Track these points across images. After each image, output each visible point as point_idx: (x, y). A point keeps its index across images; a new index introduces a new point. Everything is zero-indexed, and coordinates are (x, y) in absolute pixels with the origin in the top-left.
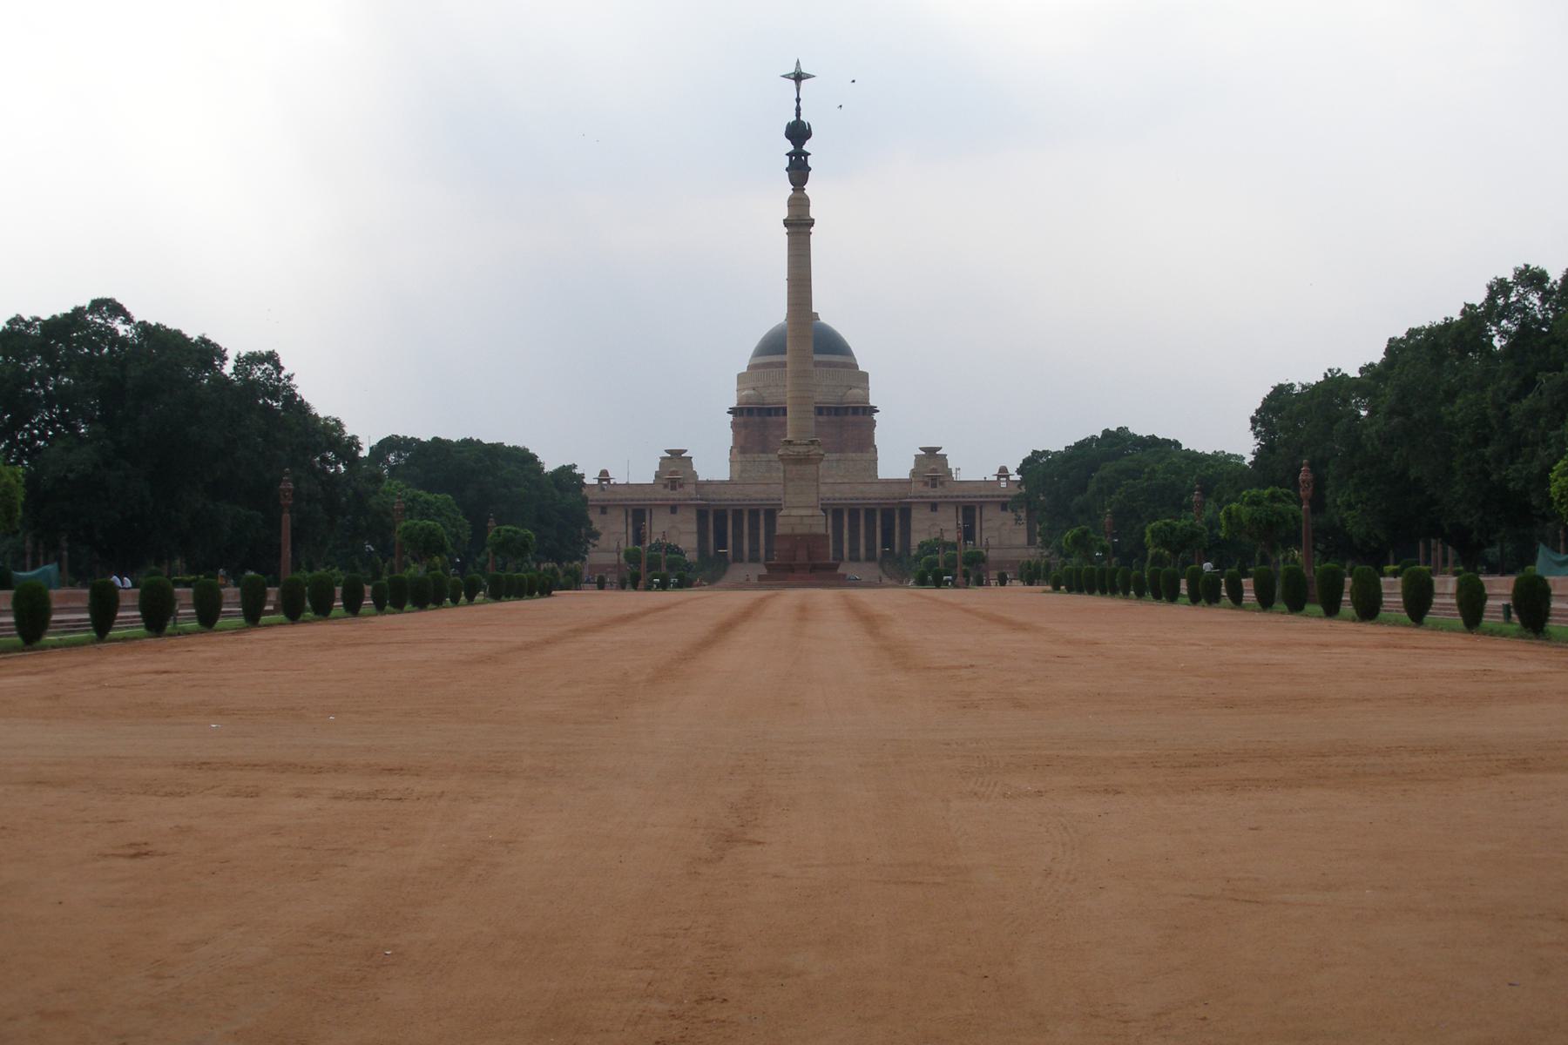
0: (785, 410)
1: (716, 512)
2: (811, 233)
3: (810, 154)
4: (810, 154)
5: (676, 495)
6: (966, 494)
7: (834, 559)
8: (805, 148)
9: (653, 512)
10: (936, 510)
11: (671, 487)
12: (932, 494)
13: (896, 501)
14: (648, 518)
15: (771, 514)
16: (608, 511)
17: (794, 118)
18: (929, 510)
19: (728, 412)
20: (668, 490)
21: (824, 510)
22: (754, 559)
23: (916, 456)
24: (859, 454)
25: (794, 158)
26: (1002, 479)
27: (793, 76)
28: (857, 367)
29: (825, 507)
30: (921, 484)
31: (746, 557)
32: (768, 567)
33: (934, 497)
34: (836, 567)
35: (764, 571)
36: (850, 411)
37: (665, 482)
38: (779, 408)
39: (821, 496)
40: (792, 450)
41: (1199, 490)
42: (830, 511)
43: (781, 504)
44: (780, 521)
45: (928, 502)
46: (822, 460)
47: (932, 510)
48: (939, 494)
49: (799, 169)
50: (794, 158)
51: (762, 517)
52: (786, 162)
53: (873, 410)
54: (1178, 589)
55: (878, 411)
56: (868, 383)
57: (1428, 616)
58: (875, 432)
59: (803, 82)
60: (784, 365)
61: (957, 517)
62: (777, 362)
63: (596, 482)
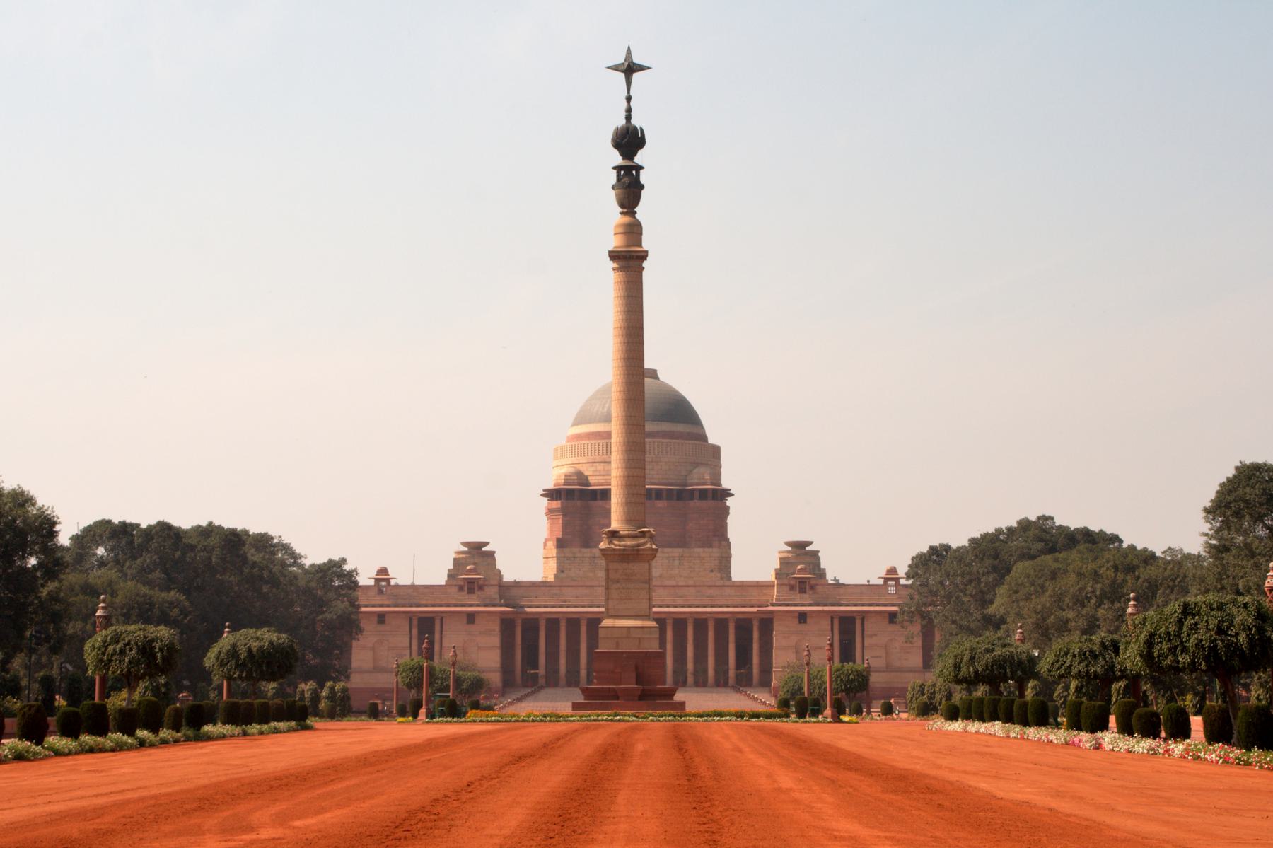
3: (642, 168)
4: (642, 168)
8: (639, 158)
10: (805, 622)
11: (468, 589)
17: (622, 122)
19: (542, 495)
22: (572, 681)
23: (614, 168)
25: (622, 172)
26: (890, 583)
28: (704, 438)
30: (786, 588)
32: (587, 693)
41: (1134, 599)
45: (885, 612)
50: (622, 172)
52: (612, 177)
53: (726, 494)
55: (732, 495)
58: (728, 521)
59: (636, 76)
60: (608, 435)
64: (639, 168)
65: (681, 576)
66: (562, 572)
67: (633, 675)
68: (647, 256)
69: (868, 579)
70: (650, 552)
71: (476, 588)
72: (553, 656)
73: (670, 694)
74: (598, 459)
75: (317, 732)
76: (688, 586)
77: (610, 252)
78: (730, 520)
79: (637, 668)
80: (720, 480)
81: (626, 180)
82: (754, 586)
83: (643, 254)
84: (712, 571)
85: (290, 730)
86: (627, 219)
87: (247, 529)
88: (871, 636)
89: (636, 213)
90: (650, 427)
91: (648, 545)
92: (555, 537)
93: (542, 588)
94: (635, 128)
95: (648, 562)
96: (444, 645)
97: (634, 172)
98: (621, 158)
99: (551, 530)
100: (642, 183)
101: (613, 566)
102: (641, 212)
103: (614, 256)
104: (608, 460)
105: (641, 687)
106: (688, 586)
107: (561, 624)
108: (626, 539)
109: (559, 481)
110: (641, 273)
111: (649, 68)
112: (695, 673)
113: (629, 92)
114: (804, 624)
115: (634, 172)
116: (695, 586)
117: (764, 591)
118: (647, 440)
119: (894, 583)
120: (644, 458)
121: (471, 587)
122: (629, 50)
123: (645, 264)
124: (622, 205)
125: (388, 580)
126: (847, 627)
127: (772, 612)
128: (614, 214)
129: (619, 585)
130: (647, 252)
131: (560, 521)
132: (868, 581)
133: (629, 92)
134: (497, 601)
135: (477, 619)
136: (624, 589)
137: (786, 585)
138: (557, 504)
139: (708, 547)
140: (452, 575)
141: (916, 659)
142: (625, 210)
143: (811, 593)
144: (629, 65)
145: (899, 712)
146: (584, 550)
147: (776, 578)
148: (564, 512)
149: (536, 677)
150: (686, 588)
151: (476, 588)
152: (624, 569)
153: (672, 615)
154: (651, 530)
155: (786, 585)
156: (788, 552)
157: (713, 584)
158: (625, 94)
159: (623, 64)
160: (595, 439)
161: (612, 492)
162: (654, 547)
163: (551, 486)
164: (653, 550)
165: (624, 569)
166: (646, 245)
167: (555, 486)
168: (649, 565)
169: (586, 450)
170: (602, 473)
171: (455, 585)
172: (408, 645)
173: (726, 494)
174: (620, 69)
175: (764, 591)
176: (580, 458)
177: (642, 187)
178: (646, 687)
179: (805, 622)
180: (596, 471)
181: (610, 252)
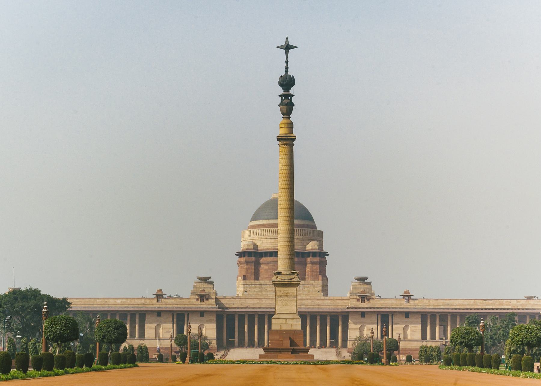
2: (294, 144)
3: (294, 96)
4: (294, 96)
6: (383, 306)
8: (291, 92)
10: (364, 317)
12: (361, 306)
13: (340, 310)
16: (410, 316)
19: (236, 255)
20: (199, 302)
22: (261, 344)
23: (279, 96)
24: (316, 281)
25: (284, 98)
27: (284, 47)
28: (315, 227)
30: (355, 300)
33: (363, 308)
37: (197, 297)
40: (280, 278)
41: (46, 305)
43: (274, 312)
44: (273, 321)
45: (404, 312)
46: (299, 284)
47: (406, 317)
48: (366, 306)
51: (256, 320)
52: (279, 100)
53: (326, 254)
55: (329, 255)
60: (276, 226)
61: (377, 321)
62: (267, 224)
63: (155, 296)
65: (303, 294)
66: (246, 292)
67: (289, 342)
72: (241, 332)
73: (307, 350)
75: (310, 367)
76: (307, 299)
79: (290, 338)
83: (293, 137)
84: (319, 292)
85: (130, 367)
86: (286, 121)
89: (290, 117)
90: (296, 222)
92: (242, 275)
93: (237, 300)
97: (289, 98)
99: (240, 271)
101: (278, 289)
102: (293, 117)
103: (279, 139)
106: (307, 299)
107: (245, 317)
109: (244, 248)
113: (287, 59)
114: (364, 318)
115: (289, 98)
117: (344, 302)
120: (294, 237)
122: (287, 39)
124: (283, 114)
127: (348, 312)
128: (279, 117)
129: (281, 298)
132: (341, 297)
133: (287, 59)
134: (215, 306)
136: (284, 300)
137: (355, 299)
139: (317, 280)
140: (192, 294)
143: (367, 302)
145: (415, 360)
146: (256, 281)
150: (306, 300)
152: (284, 291)
153: (268, 313)
155: (195, 298)
157: (319, 298)
158: (285, 60)
161: (278, 253)
163: (241, 251)
165: (284, 291)
166: (295, 134)
167: (242, 250)
169: (257, 233)
171: (195, 298)
174: (283, 48)
175: (344, 302)
176: (302, 236)
177: (293, 105)
178: (295, 348)
179: (364, 317)
180: (262, 243)
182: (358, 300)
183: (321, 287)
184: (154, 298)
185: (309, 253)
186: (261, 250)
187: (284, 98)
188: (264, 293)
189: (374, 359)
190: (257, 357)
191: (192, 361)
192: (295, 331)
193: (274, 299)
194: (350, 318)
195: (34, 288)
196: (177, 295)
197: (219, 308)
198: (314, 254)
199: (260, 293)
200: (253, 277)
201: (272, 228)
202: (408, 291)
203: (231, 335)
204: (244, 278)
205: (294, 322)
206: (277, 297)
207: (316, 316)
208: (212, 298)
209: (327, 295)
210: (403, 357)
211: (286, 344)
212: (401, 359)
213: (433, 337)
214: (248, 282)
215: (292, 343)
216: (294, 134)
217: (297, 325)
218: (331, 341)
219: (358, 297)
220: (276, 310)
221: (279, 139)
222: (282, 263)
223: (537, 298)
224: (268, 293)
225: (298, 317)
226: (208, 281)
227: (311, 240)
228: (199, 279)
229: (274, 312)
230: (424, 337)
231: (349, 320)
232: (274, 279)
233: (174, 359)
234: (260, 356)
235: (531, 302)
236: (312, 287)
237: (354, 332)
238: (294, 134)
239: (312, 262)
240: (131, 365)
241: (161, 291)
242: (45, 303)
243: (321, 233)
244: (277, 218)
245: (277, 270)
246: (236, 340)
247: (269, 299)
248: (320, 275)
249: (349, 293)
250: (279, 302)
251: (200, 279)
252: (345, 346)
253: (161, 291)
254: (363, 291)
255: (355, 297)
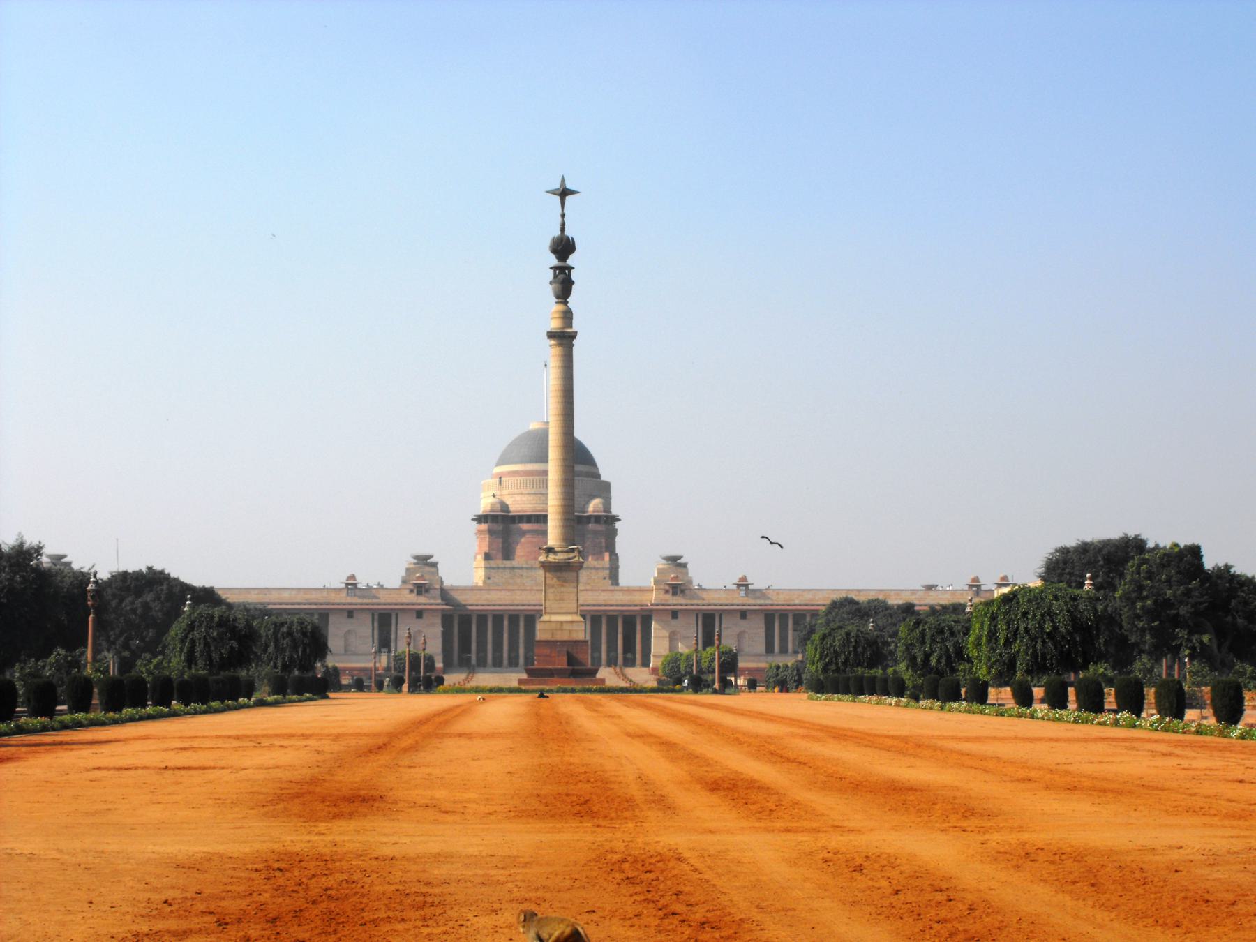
0: (546, 516)
1: (461, 617)
2: (573, 345)
3: (573, 268)
4: (573, 268)
5: (677, 601)
7: (592, 665)
9: (723, 617)
11: (673, 592)
12: (671, 602)
14: (393, 621)
15: (531, 619)
16: (355, 615)
18: (670, 617)
19: (473, 520)
21: (584, 616)
22: (513, 663)
23: (551, 268)
24: (600, 562)
25: (558, 271)
26: (741, 588)
28: (598, 476)
29: (583, 613)
30: (663, 592)
31: (505, 662)
32: (531, 672)
34: (595, 672)
35: (524, 676)
36: (593, 520)
38: (540, 515)
39: (581, 602)
40: (552, 558)
41: (190, 600)
42: (588, 617)
43: (542, 610)
44: (539, 626)
49: (564, 285)
51: (506, 623)
53: (615, 519)
54: (1066, 696)
55: (619, 520)
56: (610, 492)
57: (450, 743)
58: (616, 540)
59: (568, 198)
62: (522, 471)
63: (343, 585)
64: (570, 268)
66: (489, 578)
67: (565, 658)
68: (576, 336)
69: (725, 585)
70: (578, 564)
71: (679, 592)
74: (516, 491)
76: (587, 590)
77: (548, 332)
78: (618, 539)
80: (610, 508)
81: (561, 277)
82: (638, 590)
83: (573, 334)
84: (605, 578)
87: (1143, 537)
88: (727, 628)
91: (577, 558)
94: (568, 238)
95: (577, 572)
96: (398, 635)
97: (567, 271)
98: (557, 260)
99: (480, 547)
100: (573, 279)
102: (572, 301)
103: (551, 335)
104: (544, 492)
105: (571, 668)
106: (587, 590)
108: (559, 554)
110: (572, 349)
111: (578, 192)
112: (510, 658)
115: (567, 271)
116: (592, 590)
118: (576, 478)
119: (744, 588)
121: (420, 589)
122: (563, 180)
123: (575, 342)
124: (558, 297)
125: (355, 585)
126: (709, 621)
128: (554, 307)
130: (576, 332)
131: (487, 539)
135: (425, 615)
138: (484, 526)
140: (404, 582)
141: (761, 647)
142: (560, 300)
144: (563, 190)
146: (505, 562)
147: (654, 584)
148: (491, 532)
149: (469, 659)
151: (679, 592)
154: (580, 547)
156: (415, 564)
159: (558, 189)
160: (510, 477)
162: (581, 560)
163: (480, 513)
164: (580, 562)
168: (578, 574)
170: (526, 502)
172: (371, 634)
173: (615, 519)
178: (576, 668)
180: (515, 501)
181: (548, 332)
182: (667, 592)
183: (608, 572)
184: (343, 588)
185: (589, 517)
186: (514, 512)
187: (558, 271)
188: (518, 581)
189: (699, 685)
190: (515, 684)
191: (414, 689)
192: (576, 643)
193: (542, 590)
194: (654, 618)
195: (158, 567)
196: (379, 584)
197: (447, 605)
198: (597, 519)
199: (511, 581)
200: (500, 555)
201: (531, 478)
202: (745, 577)
203: (465, 646)
204: (487, 557)
205: (575, 627)
206: (547, 587)
207: (600, 617)
208: (435, 589)
209: (617, 584)
210: (741, 681)
211: (562, 663)
212: (738, 683)
213: (784, 650)
214: (492, 563)
215: (571, 660)
216: (575, 328)
217: (581, 632)
218: (505, 662)
219: (667, 588)
220: (545, 608)
221: (551, 335)
222: (553, 535)
223: (942, 587)
224: (525, 581)
225: (580, 619)
226: (429, 561)
227: (594, 497)
228: (923, 587)
229: (542, 610)
230: (769, 649)
231: (653, 623)
232: (542, 558)
233: (380, 687)
234: (521, 681)
235: (932, 593)
236: (593, 571)
237: (659, 646)
238: (575, 328)
239: (595, 533)
240: (279, 697)
241: (353, 577)
242: (189, 596)
243: (607, 486)
244: (547, 461)
245: (547, 544)
246: (474, 656)
247: (527, 590)
248: (606, 551)
249: (652, 580)
250: (550, 596)
251: (417, 557)
252: (646, 663)
253: (353, 577)
254: (674, 577)
255: (662, 587)
